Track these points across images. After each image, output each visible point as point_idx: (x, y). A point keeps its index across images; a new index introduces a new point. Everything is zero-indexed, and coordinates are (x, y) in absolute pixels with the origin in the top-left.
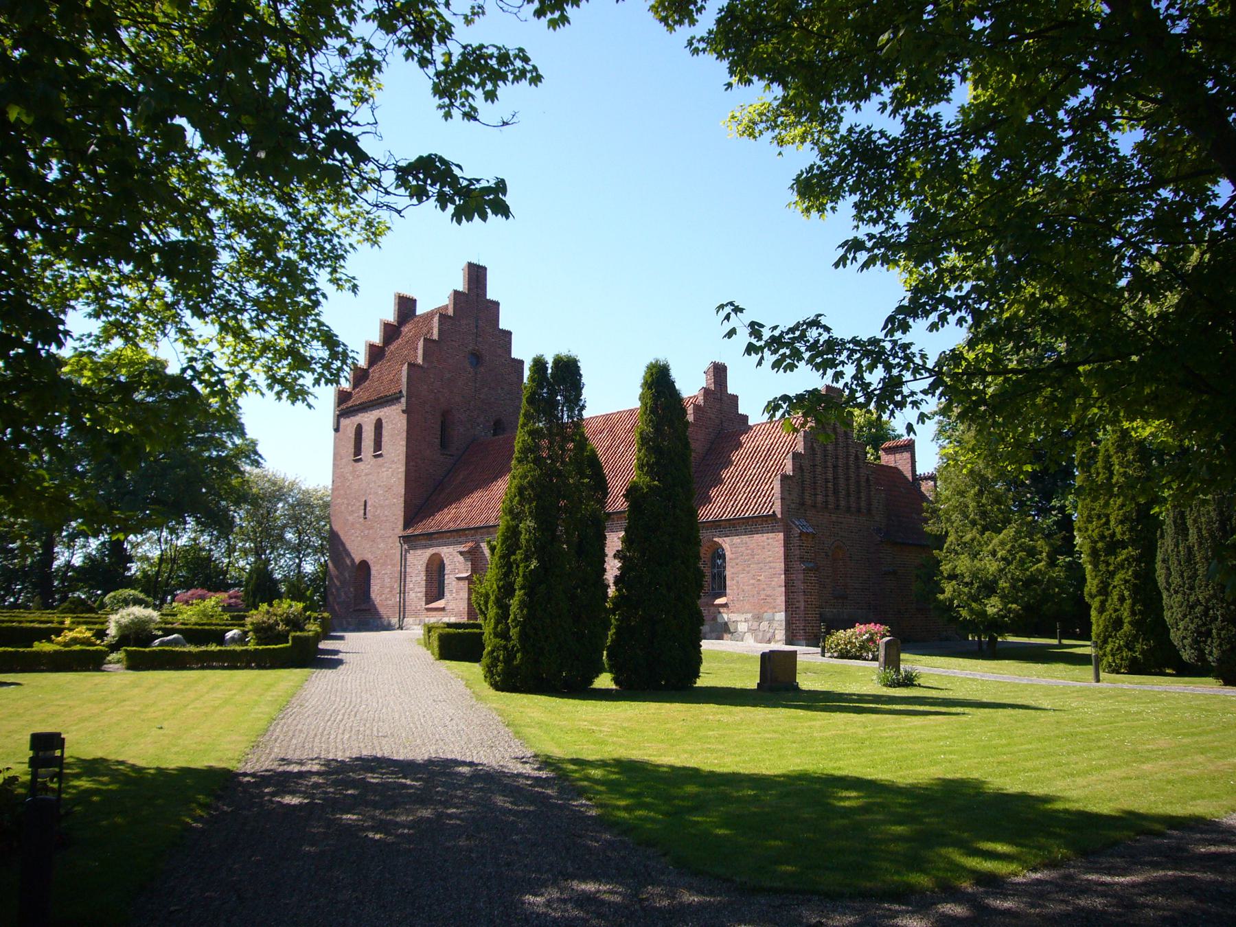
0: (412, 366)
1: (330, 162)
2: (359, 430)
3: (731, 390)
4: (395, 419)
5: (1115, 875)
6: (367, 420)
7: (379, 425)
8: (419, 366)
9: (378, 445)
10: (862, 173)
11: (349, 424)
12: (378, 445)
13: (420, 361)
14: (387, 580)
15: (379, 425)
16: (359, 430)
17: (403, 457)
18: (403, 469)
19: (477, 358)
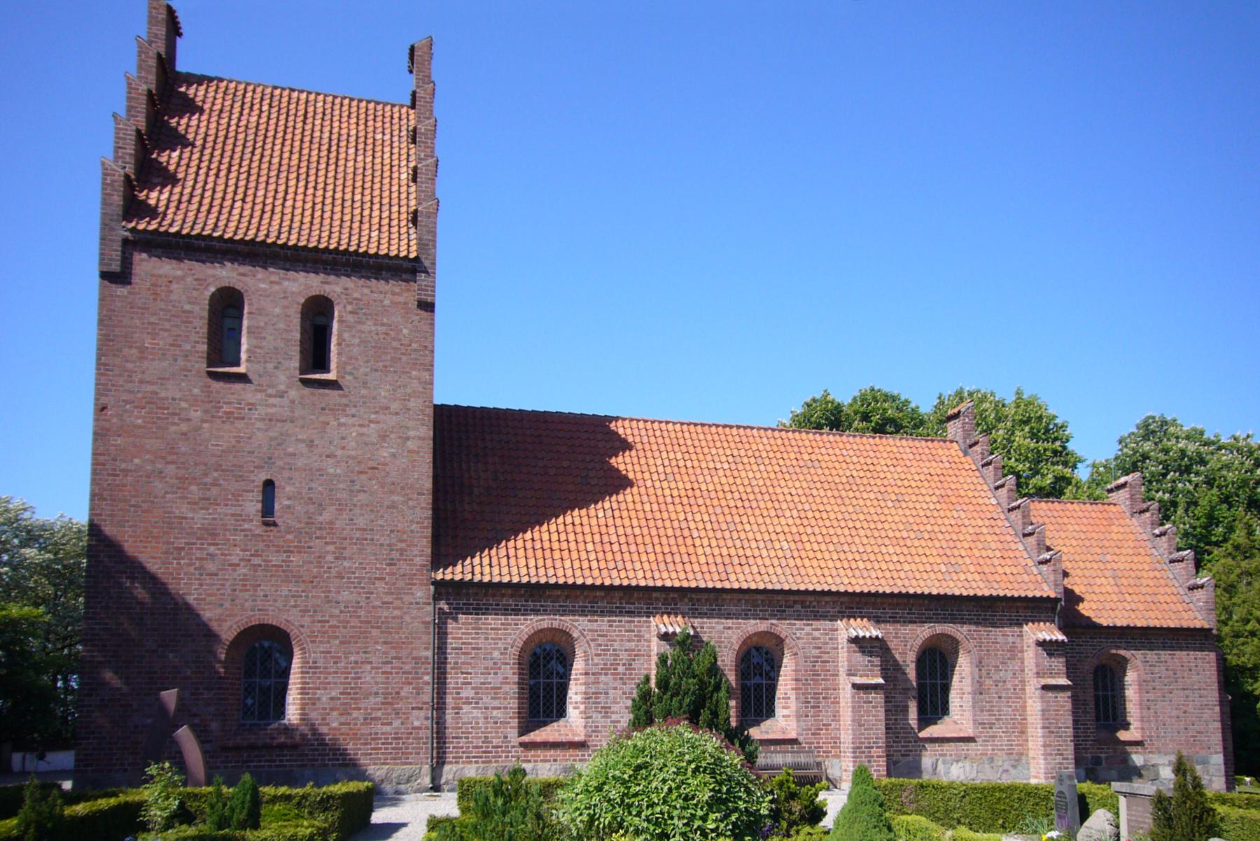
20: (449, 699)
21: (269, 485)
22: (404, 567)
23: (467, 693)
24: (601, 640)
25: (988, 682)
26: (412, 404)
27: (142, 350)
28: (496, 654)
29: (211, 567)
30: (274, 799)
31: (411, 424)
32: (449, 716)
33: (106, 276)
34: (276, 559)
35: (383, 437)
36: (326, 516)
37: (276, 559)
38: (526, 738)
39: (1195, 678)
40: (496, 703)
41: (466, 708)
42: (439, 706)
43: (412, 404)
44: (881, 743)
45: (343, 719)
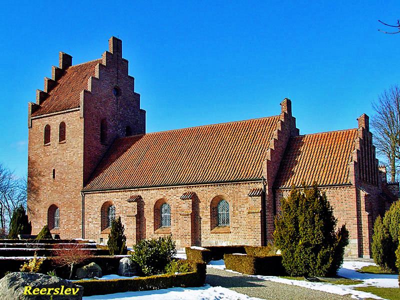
0: (86, 92)
1: (267, 192)
2: (48, 129)
3: (124, 56)
4: (75, 121)
5: (292, 286)
6: (54, 122)
7: (63, 126)
8: (89, 92)
9: (62, 137)
10: (326, 205)
11: (40, 125)
12: (62, 137)
13: (89, 89)
14: (72, 216)
15: (63, 126)
16: (48, 129)
17: (81, 145)
18: (82, 151)
19: (117, 91)
20: (86, 222)
21: (54, 170)
22: (78, 188)
23: (90, 220)
24: (119, 204)
25: (237, 212)
26: (79, 145)
27: (35, 143)
28: (96, 209)
29: (45, 191)
30: (64, 293)
31: (79, 150)
32: (86, 226)
33: (29, 128)
34: (55, 188)
35: (74, 154)
36: (64, 176)
37: (55, 188)
38: (102, 232)
39: (345, 206)
40: (96, 223)
41: (90, 224)
42: (83, 223)
43: (79, 145)
44: (190, 234)
45: (67, 227)
